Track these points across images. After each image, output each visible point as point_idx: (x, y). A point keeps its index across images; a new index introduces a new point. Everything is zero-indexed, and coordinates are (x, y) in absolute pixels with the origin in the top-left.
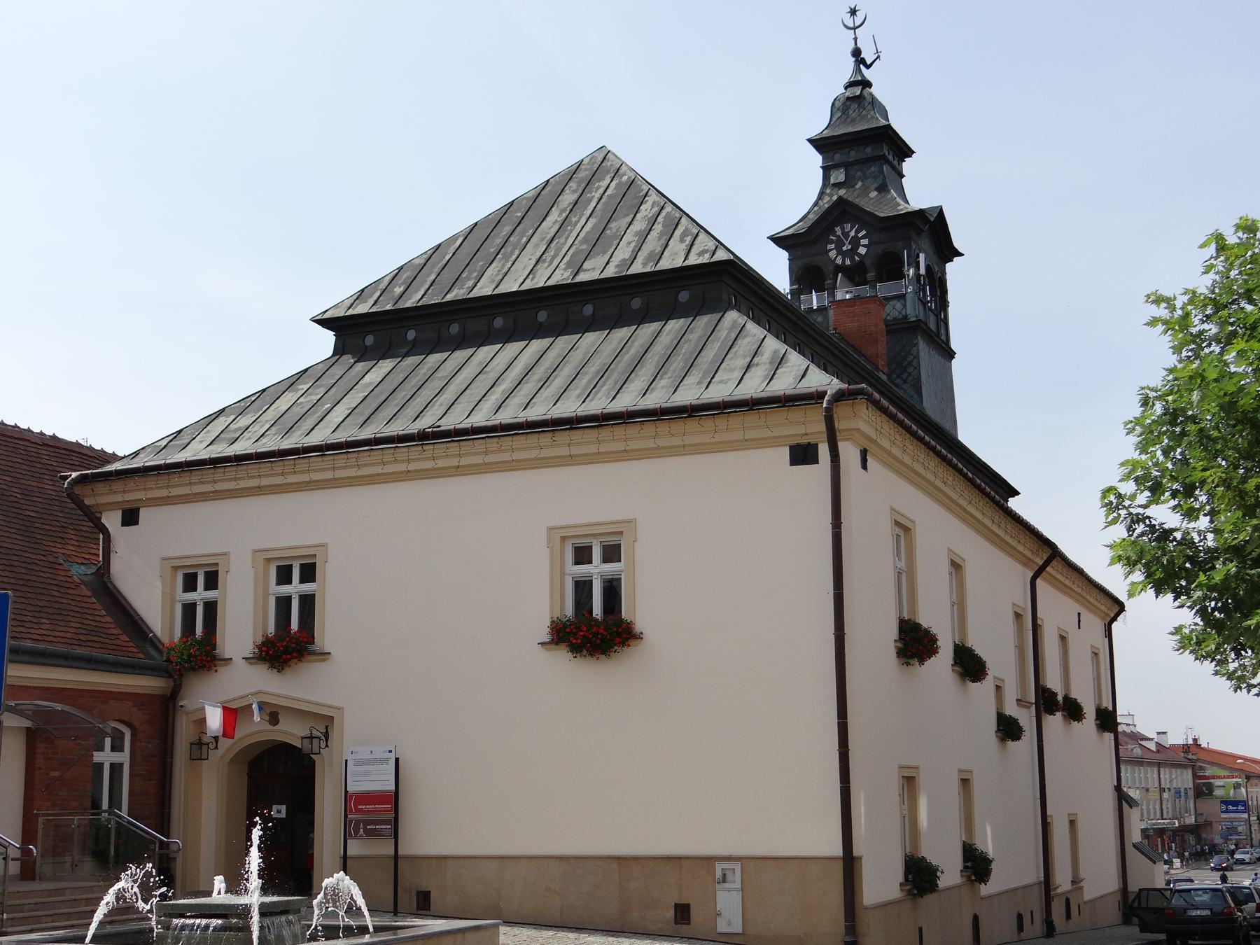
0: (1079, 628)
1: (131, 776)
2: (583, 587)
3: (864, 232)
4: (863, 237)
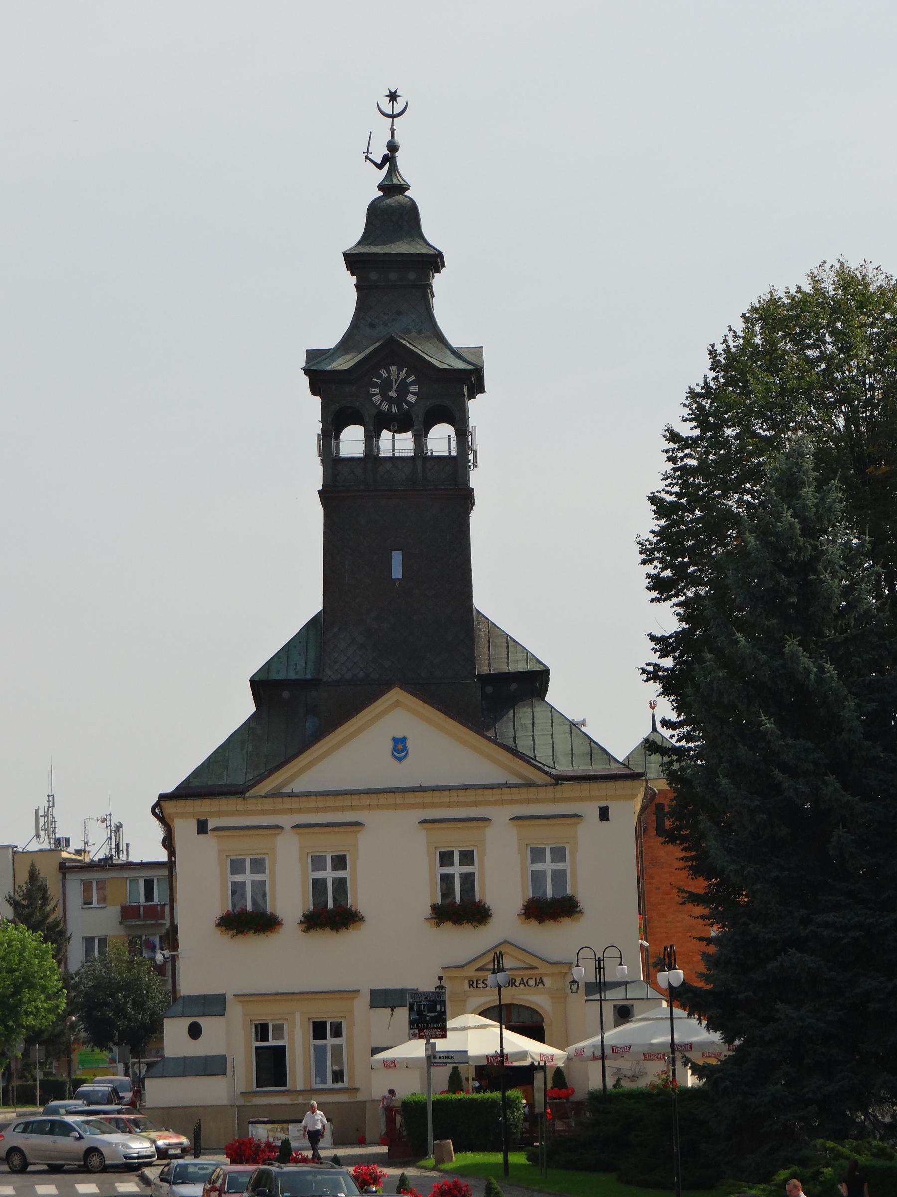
0: (371, 133)
1: (270, 1105)
2: (447, 880)
3: (412, 378)
4: (412, 383)
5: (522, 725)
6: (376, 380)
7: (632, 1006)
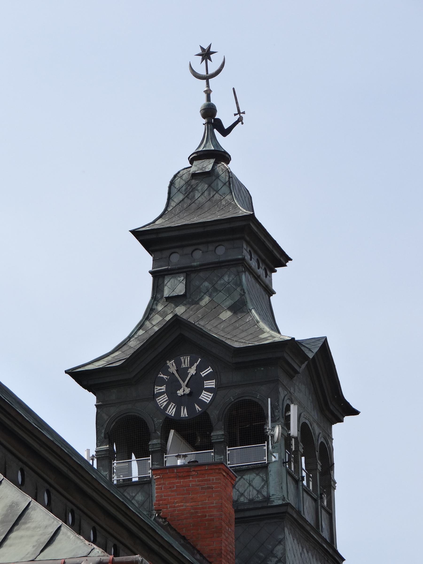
0: (234, 89)
3: (209, 370)
6: (162, 376)
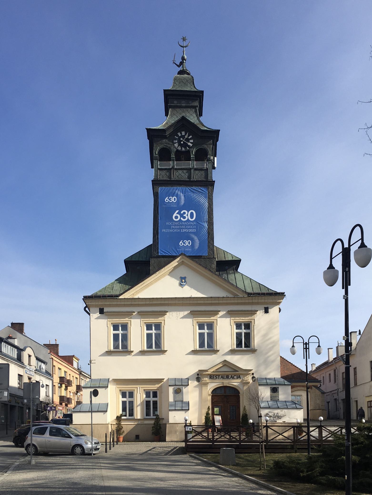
3: (191, 137)
5: (231, 279)
7: (278, 387)
